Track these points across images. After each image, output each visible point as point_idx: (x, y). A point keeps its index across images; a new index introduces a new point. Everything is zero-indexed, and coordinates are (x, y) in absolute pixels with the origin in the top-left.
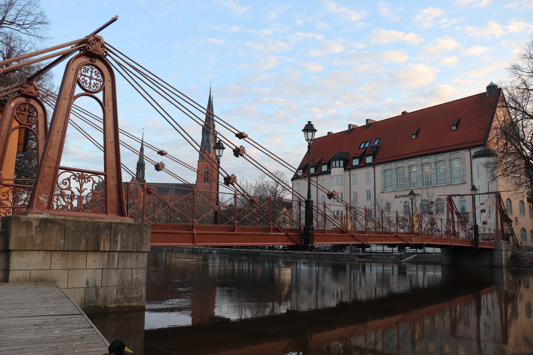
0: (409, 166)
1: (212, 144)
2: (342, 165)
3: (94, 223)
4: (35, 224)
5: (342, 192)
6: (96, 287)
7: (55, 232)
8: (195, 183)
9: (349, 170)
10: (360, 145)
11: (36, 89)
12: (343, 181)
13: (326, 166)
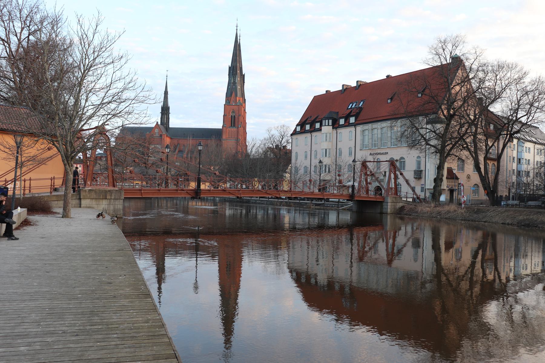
0: (382, 127)
1: (239, 87)
2: (330, 124)
3: (105, 190)
4: (87, 191)
5: (330, 147)
6: (106, 210)
7: (93, 193)
8: (222, 128)
9: (336, 128)
11: (81, 135)
12: (331, 138)
13: (319, 123)
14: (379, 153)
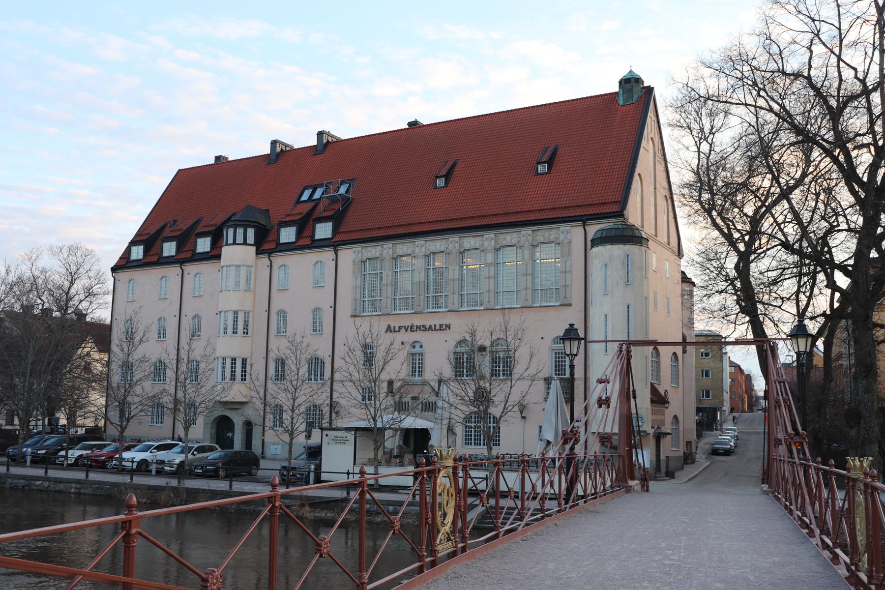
2: (251, 239)
5: (248, 308)
9: (270, 253)
14: (418, 328)
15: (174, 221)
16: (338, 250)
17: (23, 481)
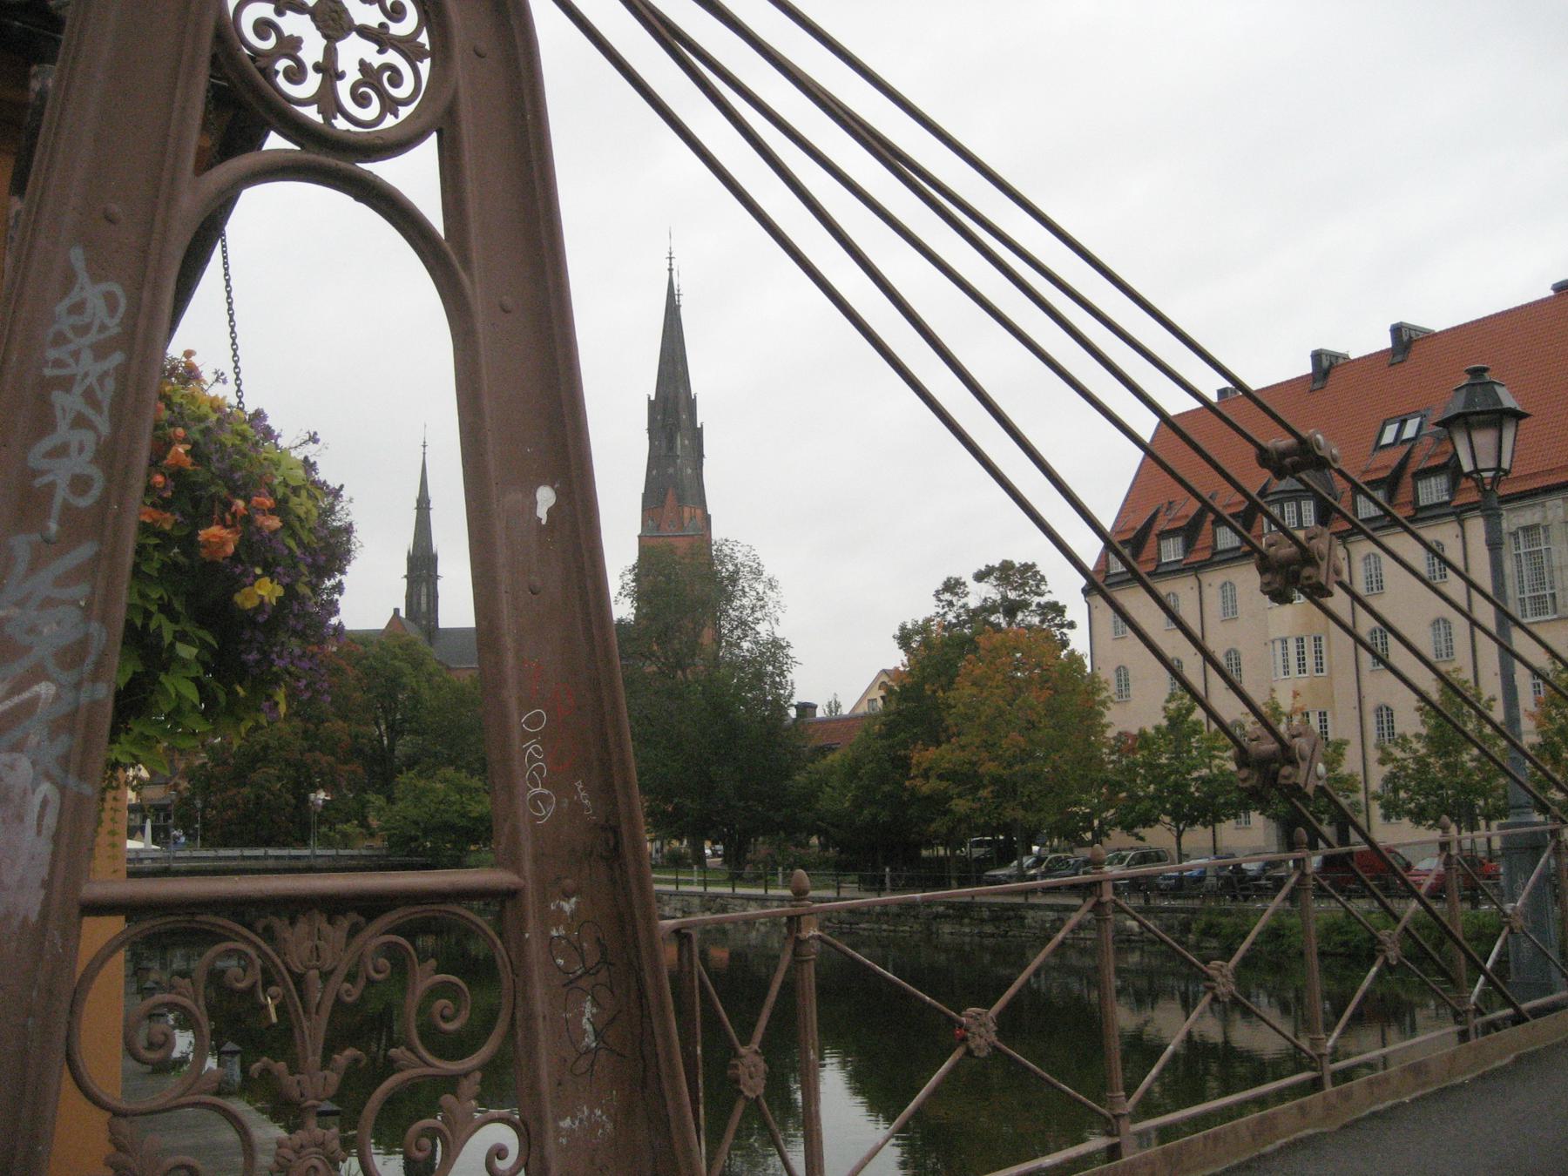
10: (1377, 434)
15: (1170, 503)
16: (1463, 520)
17: (1051, 913)
